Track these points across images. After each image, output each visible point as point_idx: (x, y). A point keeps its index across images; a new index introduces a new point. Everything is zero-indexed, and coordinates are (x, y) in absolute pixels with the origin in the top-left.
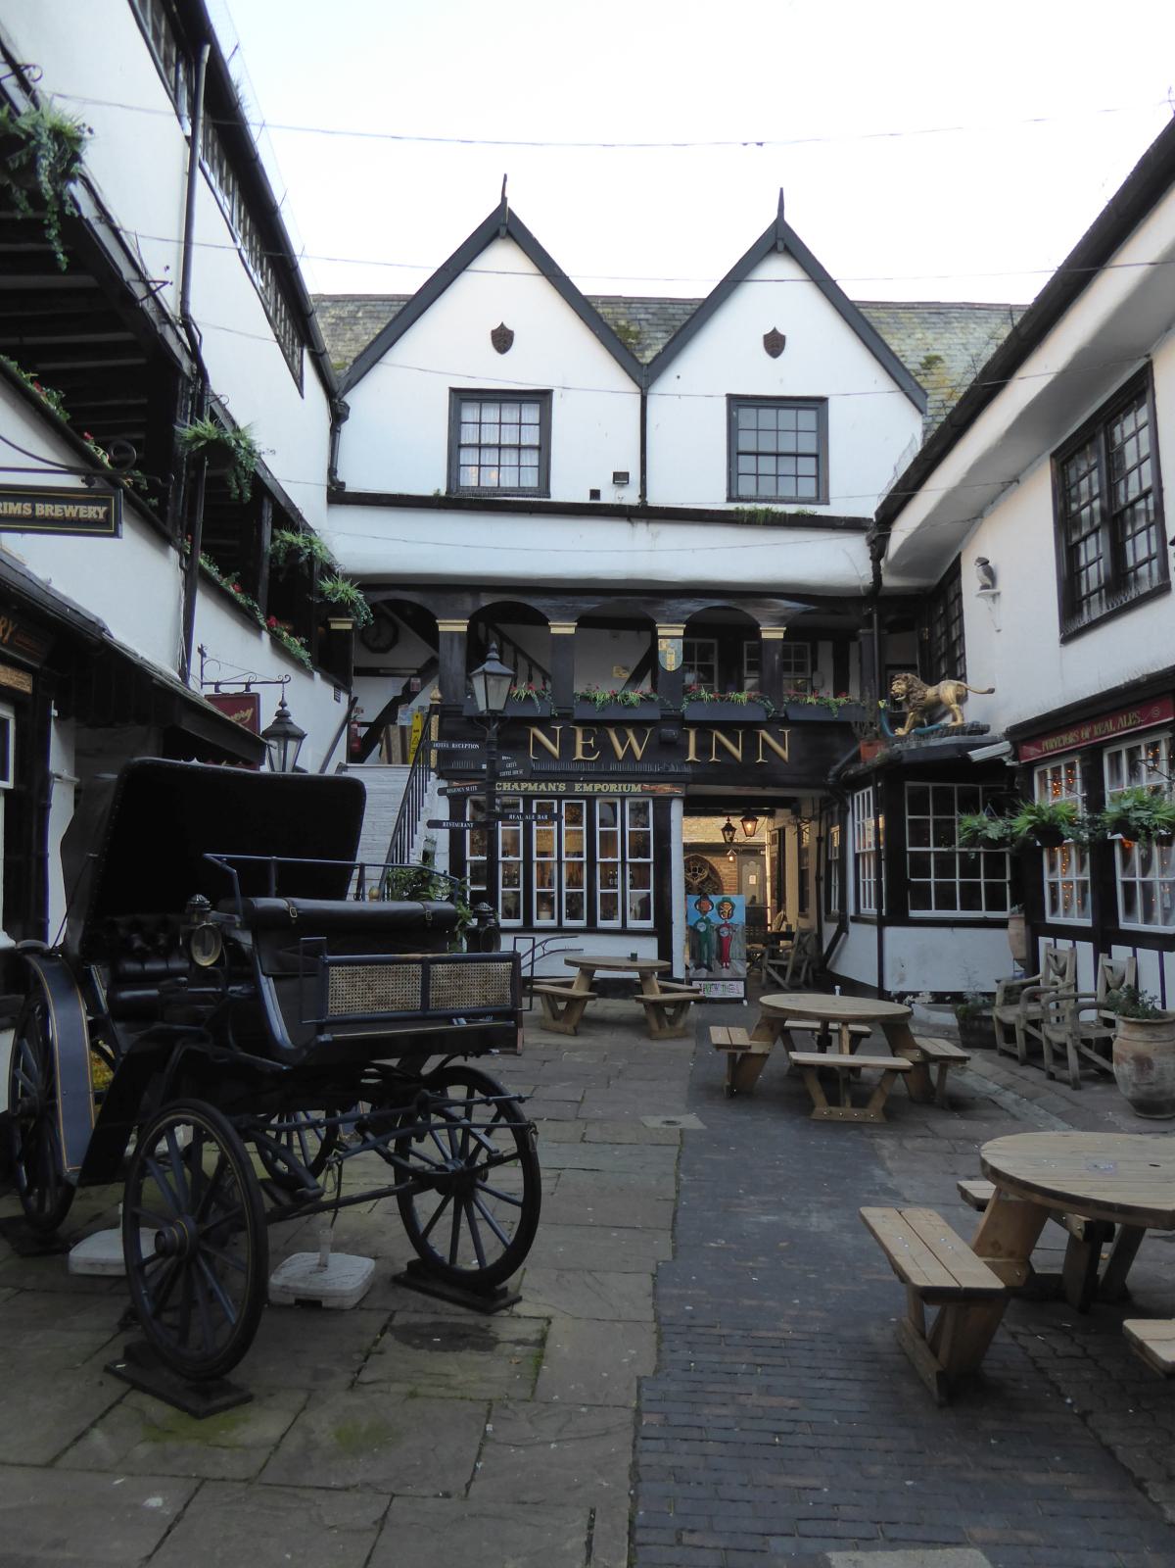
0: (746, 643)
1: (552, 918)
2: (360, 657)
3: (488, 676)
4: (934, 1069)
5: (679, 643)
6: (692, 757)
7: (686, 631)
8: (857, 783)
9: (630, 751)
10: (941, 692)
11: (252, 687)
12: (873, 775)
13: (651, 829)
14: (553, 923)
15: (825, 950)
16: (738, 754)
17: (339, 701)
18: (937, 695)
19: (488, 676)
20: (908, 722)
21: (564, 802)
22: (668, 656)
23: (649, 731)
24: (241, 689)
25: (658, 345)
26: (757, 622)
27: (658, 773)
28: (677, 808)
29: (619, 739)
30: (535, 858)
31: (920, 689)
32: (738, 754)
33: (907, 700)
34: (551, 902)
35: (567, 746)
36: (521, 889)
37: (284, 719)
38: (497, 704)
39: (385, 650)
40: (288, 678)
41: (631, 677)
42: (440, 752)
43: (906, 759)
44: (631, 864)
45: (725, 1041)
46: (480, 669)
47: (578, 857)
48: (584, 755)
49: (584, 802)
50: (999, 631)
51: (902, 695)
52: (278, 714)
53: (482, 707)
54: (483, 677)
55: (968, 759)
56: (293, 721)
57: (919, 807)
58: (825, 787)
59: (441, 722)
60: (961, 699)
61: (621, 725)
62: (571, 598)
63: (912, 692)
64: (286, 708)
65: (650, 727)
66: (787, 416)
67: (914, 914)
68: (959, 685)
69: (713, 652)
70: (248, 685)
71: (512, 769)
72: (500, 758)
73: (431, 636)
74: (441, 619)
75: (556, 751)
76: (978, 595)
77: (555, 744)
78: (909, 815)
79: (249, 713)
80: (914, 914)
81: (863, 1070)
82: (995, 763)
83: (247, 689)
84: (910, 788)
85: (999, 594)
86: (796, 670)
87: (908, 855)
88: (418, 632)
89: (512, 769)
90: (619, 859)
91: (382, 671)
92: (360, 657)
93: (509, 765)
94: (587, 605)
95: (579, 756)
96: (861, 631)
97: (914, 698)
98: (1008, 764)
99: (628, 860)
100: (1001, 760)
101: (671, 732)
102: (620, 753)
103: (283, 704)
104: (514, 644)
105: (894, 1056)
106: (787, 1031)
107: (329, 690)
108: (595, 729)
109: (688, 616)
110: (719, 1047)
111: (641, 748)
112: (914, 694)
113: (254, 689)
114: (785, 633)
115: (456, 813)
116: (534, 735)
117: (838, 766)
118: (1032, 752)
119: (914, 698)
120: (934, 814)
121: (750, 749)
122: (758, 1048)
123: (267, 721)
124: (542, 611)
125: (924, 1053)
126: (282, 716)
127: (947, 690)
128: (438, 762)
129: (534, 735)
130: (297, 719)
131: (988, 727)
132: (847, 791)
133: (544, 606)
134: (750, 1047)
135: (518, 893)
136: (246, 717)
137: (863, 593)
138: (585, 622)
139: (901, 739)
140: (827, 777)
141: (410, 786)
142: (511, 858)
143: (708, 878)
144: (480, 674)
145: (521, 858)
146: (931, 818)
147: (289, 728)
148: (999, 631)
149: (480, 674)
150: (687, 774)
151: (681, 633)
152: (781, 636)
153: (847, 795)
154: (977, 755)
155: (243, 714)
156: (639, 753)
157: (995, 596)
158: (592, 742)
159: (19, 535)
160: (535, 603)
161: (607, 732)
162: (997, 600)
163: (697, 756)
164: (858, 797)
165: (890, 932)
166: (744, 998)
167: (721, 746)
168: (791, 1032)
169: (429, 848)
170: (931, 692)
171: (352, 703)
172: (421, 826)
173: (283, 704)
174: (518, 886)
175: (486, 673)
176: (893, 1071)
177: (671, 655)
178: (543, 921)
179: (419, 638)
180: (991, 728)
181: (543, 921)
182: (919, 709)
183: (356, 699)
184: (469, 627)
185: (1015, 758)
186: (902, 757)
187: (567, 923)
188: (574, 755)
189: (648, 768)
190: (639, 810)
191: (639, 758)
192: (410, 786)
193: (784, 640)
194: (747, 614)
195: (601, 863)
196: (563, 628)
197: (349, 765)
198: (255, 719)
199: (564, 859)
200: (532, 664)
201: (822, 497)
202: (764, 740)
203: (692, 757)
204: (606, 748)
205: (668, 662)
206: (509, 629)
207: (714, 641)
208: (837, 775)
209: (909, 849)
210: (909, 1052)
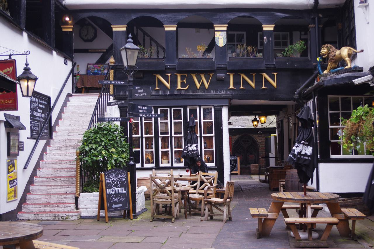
0: (245, 33)
1: (169, 163)
2: (78, 44)
3: (127, 50)
4: (350, 222)
5: (225, 34)
6: (231, 87)
7: (228, 28)
9: (203, 84)
10: (342, 54)
12: (313, 93)
13: (213, 120)
14: (169, 165)
16: (253, 85)
17: (67, 64)
18: (340, 54)
19: (127, 50)
20: (329, 67)
21: (172, 109)
22: (220, 40)
23: (211, 75)
24: (7, 58)
26: (261, 23)
27: (215, 95)
28: (225, 112)
29: (197, 79)
30: (160, 135)
31: (333, 51)
32: (253, 85)
33: (328, 57)
34: (167, 155)
35: (174, 83)
36: (154, 150)
38: (133, 63)
39: (91, 40)
40: (29, 52)
41: (205, 51)
42: (115, 86)
43: (326, 84)
44: (204, 137)
45: (257, 213)
46: (124, 47)
47: (179, 134)
48: (181, 87)
49: (182, 109)
50: (368, 23)
51: (325, 55)
52: (25, 69)
53: (125, 64)
54: (125, 50)
55: (353, 83)
56: (32, 72)
57: (335, 106)
58: (294, 100)
60: (353, 57)
61: (198, 73)
62: (174, 14)
63: (330, 53)
64: (28, 66)
65: (211, 73)
67: (333, 157)
68: (349, 49)
69: (243, 38)
70: (10, 56)
71: (141, 93)
72: (134, 88)
73: (110, 33)
74: (114, 25)
75: (168, 85)
76: (359, 6)
77: (168, 82)
78: (330, 111)
79: (11, 69)
80: (333, 157)
81: (317, 224)
82: (365, 85)
83: (10, 58)
84: (331, 99)
85: (368, 5)
86: (283, 45)
87: (330, 130)
88: (104, 31)
89: (141, 93)
91: (90, 51)
92: (78, 44)
93: (140, 91)
94: (182, 17)
95: (179, 87)
96: (310, 26)
97: (331, 56)
98: (371, 85)
99: (203, 135)
100: (368, 84)
101: (221, 75)
102: (198, 85)
103: (27, 65)
105: (333, 217)
106: (284, 210)
107: (61, 60)
108: (186, 75)
109: (229, 21)
110: (253, 216)
111: (168, 83)
112: (331, 54)
113: (13, 58)
114: (274, 28)
116: (158, 78)
117: (300, 89)
119: (331, 56)
120: (342, 110)
121: (258, 82)
122: (271, 216)
123: (20, 71)
124: (161, 20)
125: (346, 216)
126: (27, 70)
127: (345, 51)
129: (158, 78)
130: (34, 71)
131: (362, 68)
132: (304, 101)
133: (161, 18)
134: (268, 215)
135: (153, 151)
136: (10, 71)
137: (310, 8)
138: (180, 25)
139: (325, 75)
140: (294, 94)
142: (149, 136)
144: (123, 49)
145: (153, 135)
146: (340, 112)
147: (29, 75)
148: (368, 23)
149: (123, 49)
150: (229, 94)
151: (225, 29)
152: (272, 29)
153: (304, 103)
154: (357, 81)
155: (8, 70)
156: (207, 85)
157: (366, 7)
158: (185, 81)
159: (193, 30)
161: (200, 76)
162: (367, 8)
163: (234, 86)
164: (309, 103)
166: (305, 187)
167: (245, 82)
168: (287, 210)
169: (232, 124)
170: (338, 52)
171: (74, 65)
173: (27, 65)
174: (152, 148)
176: (330, 224)
177: (221, 39)
178: (164, 164)
179: (105, 34)
180: (364, 68)
181: (164, 164)
182: (333, 61)
183: (75, 63)
186: (324, 84)
187: (175, 165)
189: (211, 92)
190: (207, 113)
191: (207, 88)
192: (98, 102)
193: (274, 30)
194: (256, 19)
197: (73, 94)
199: (173, 135)
202: (265, 78)
203: (231, 87)
205: (220, 42)
206: (148, 30)
207: (245, 33)
208: (299, 94)
209: (330, 127)
210: (339, 215)
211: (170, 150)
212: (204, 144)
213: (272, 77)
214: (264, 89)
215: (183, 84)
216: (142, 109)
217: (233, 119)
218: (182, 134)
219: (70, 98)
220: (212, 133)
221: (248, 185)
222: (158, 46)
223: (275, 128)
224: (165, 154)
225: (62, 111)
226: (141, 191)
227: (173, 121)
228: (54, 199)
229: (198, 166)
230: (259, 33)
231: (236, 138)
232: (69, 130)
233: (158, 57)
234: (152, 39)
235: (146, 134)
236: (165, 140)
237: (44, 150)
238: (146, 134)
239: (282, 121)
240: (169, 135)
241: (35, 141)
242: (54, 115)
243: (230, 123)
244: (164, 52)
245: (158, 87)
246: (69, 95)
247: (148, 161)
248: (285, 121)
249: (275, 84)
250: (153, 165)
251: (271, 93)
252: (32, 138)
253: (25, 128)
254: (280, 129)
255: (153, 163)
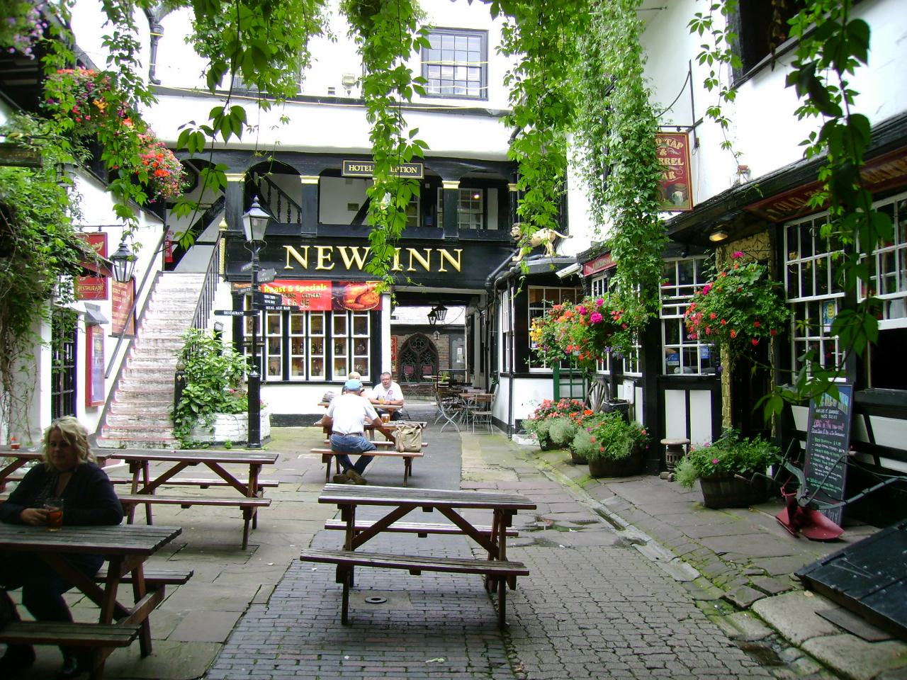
1: (301, 374)
8: (502, 286)
9: (355, 263)
11: (102, 228)
14: (303, 378)
15: (105, 371)
24: (96, 230)
25: (29, 513)
35: (313, 258)
37: (123, 249)
38: (260, 237)
48: (324, 265)
53: (249, 238)
59: (226, 243)
66: (461, 42)
67: (533, 370)
70: (100, 227)
79: (100, 245)
80: (533, 370)
83: (100, 230)
90: (347, 335)
102: (348, 264)
104: (278, 188)
113: (104, 230)
115: (237, 304)
118: (591, 270)
123: (112, 250)
128: (225, 270)
141: (205, 288)
143: (428, 350)
155: (97, 245)
160: (289, 162)
165: (517, 382)
167: (416, 262)
171: (166, 229)
172: (212, 313)
175: (251, 217)
183: (168, 226)
184: (247, 178)
185: (582, 272)
187: (312, 378)
188: (316, 265)
195: (335, 338)
196: (310, 180)
198: (104, 251)
200: (291, 202)
201: (484, 96)
204: (337, 258)
211: (304, 356)
212: (74, 362)
213: (455, 255)
214: (442, 272)
215: (326, 262)
216: (270, 299)
217: (399, 311)
218: (322, 333)
219: (160, 278)
220: (366, 333)
221: (419, 411)
222: (289, 203)
223: (463, 326)
224: (297, 362)
225: (149, 297)
226: (266, 414)
227: (353, 356)
228: (147, 423)
229: (76, 459)
230: (439, 188)
231: (403, 339)
232: (160, 325)
233: (289, 222)
234: (281, 193)
235: (270, 332)
236: (297, 342)
237: (127, 353)
238: (270, 332)
239: (473, 316)
240: (304, 335)
241: (117, 339)
242: (139, 305)
243: (393, 318)
244: (299, 213)
245: (290, 265)
246: (159, 273)
247: (273, 372)
248: (477, 315)
249: (457, 265)
250: (279, 378)
251: (452, 278)
252: (114, 335)
253: (107, 323)
254: (470, 327)
255: (279, 374)
